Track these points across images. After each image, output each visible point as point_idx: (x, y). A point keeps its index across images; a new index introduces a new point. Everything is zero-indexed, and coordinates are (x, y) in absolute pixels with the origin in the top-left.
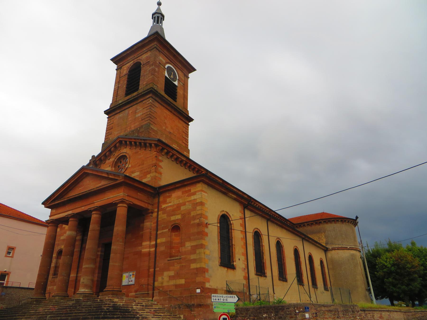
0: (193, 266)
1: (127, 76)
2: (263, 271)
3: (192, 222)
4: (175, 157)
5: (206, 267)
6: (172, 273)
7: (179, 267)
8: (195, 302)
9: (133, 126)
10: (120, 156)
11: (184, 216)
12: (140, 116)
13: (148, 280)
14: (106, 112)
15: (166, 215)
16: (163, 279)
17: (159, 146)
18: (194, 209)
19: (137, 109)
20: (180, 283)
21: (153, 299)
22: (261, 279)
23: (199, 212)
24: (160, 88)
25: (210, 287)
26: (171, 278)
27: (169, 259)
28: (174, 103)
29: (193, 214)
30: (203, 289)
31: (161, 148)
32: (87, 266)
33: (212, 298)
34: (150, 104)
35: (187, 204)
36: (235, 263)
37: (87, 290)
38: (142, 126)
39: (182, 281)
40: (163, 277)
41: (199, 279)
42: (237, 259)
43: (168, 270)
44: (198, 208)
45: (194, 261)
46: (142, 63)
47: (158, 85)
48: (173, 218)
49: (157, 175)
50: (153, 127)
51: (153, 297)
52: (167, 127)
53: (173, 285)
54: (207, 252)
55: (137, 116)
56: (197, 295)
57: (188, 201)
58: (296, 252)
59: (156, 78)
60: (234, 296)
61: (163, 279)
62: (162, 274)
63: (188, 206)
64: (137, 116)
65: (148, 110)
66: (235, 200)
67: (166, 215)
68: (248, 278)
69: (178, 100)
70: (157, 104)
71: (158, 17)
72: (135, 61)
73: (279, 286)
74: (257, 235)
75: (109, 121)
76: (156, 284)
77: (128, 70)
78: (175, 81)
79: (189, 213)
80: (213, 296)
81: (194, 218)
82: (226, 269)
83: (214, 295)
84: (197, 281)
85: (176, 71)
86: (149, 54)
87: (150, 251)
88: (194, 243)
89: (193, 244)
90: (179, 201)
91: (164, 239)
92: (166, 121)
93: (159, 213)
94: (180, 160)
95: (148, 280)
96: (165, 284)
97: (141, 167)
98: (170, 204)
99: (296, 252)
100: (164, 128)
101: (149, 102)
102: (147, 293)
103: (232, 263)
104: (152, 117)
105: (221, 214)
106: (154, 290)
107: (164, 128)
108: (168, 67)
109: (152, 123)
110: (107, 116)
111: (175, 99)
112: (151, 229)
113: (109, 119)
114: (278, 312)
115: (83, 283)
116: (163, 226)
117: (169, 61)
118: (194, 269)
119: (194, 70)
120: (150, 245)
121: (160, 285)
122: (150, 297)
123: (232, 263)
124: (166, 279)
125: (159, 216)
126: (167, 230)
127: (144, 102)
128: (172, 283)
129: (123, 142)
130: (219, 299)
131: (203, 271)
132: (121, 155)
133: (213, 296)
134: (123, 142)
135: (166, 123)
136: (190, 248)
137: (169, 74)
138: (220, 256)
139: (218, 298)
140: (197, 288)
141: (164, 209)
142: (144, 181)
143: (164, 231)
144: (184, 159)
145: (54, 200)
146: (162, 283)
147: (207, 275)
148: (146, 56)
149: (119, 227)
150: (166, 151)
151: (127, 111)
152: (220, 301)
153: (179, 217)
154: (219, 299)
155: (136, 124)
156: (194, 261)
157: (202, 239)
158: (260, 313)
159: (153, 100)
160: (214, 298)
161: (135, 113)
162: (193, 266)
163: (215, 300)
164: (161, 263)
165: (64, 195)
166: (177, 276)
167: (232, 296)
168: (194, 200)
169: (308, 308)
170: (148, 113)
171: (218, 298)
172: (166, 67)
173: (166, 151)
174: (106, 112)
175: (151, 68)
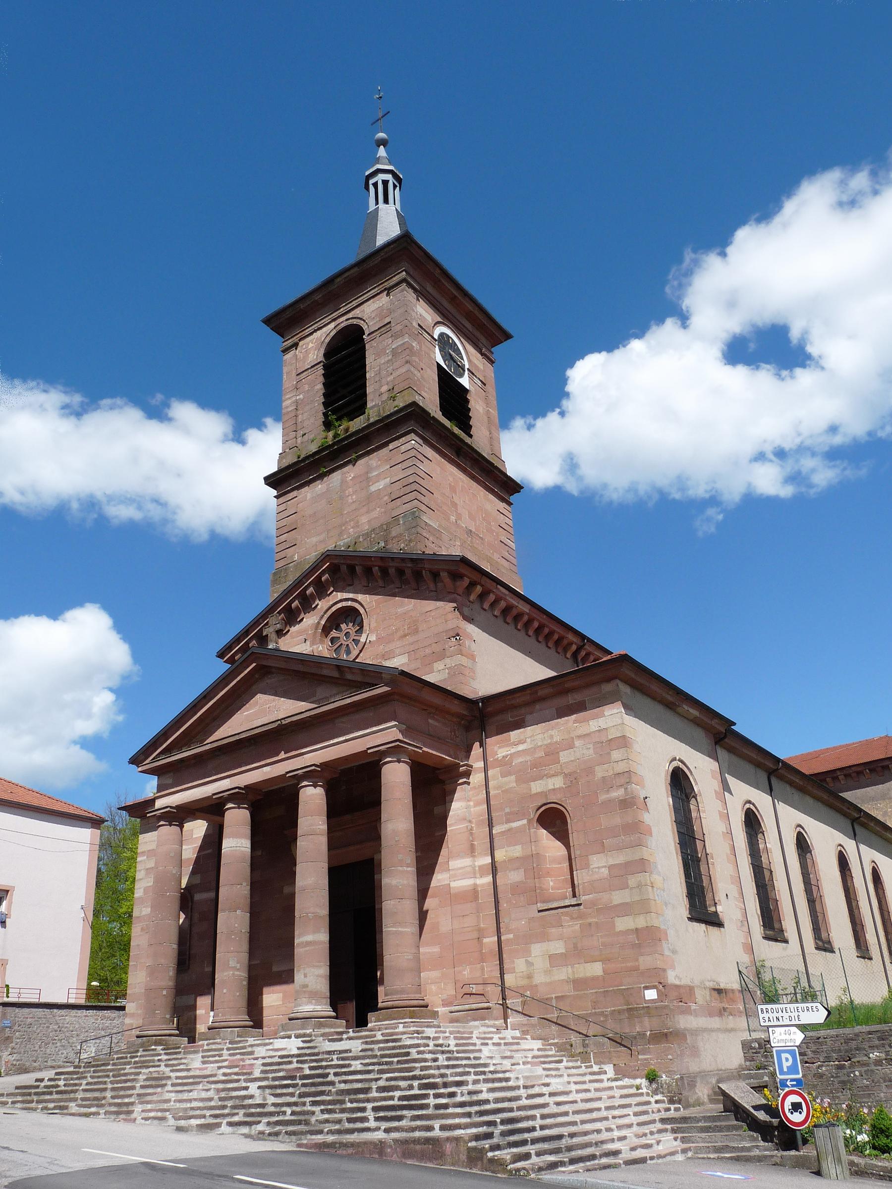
0: (623, 924)
1: (320, 371)
2: (776, 926)
3: (603, 797)
4: (503, 604)
6: (558, 947)
7: (577, 927)
8: (646, 1026)
9: (364, 520)
10: (334, 609)
11: (572, 778)
12: (385, 488)
14: (272, 481)
15: (513, 777)
16: (529, 964)
17: (461, 576)
18: (604, 758)
19: (370, 469)
20: (589, 974)
21: (506, 1022)
22: (776, 948)
23: (621, 767)
24: (430, 399)
25: (677, 982)
26: (554, 960)
27: (541, 906)
28: (468, 440)
29: (600, 772)
30: (664, 988)
31: (467, 581)
33: (761, 1016)
35: (577, 743)
36: (719, 909)
37: (319, 1008)
38: (395, 518)
39: (596, 969)
40: (529, 959)
41: (645, 962)
42: (720, 896)
43: (544, 937)
44: (616, 755)
45: (625, 909)
46: (365, 327)
47: (424, 394)
48: (537, 787)
49: (464, 661)
51: (505, 1018)
52: (459, 516)
53: (567, 981)
54: (656, 878)
55: (373, 488)
56: (649, 1009)
57: (579, 737)
58: (843, 862)
59: (416, 372)
61: (529, 964)
62: (528, 952)
63: (583, 751)
64: (373, 488)
66: (696, 722)
67: (513, 777)
68: (750, 949)
69: (473, 431)
71: (385, 183)
72: (343, 322)
73: (818, 961)
74: (752, 822)
75: (282, 507)
76: (509, 979)
77: (322, 351)
78: (461, 376)
79: (589, 770)
81: (607, 784)
84: (642, 968)
87: (475, 885)
88: (619, 858)
89: (611, 862)
90: (552, 737)
91: (519, 848)
93: (490, 773)
94: (514, 612)
95: (483, 969)
96: (539, 979)
97: (410, 639)
98: (521, 747)
99: (843, 862)
101: (408, 446)
103: (713, 909)
104: (423, 491)
105: (671, 769)
107: (453, 518)
108: (442, 335)
109: (424, 508)
110: (275, 492)
111: (466, 427)
112: (470, 822)
113: (282, 500)
116: (507, 810)
118: (628, 932)
119: (508, 336)
120: (474, 867)
121: (524, 982)
122: (496, 1019)
125: (491, 784)
126: (525, 822)
127: (391, 446)
128: (563, 974)
129: (344, 568)
130: (778, 1019)
131: (649, 937)
132: (339, 605)
134: (344, 568)
135: (455, 505)
136: (605, 871)
137: (448, 357)
139: (775, 1015)
140: (647, 988)
141: (505, 763)
142: (430, 678)
143: (515, 825)
145: (168, 751)
146: (530, 977)
147: (666, 948)
149: (397, 820)
150: (479, 589)
151: (336, 476)
153: (557, 782)
154: (778, 1019)
155: (375, 514)
156: (625, 909)
157: (640, 844)
160: (766, 1015)
161: (366, 479)
162: (623, 924)
164: (517, 919)
166: (576, 953)
173: (479, 589)
174: (272, 481)
175: (399, 342)
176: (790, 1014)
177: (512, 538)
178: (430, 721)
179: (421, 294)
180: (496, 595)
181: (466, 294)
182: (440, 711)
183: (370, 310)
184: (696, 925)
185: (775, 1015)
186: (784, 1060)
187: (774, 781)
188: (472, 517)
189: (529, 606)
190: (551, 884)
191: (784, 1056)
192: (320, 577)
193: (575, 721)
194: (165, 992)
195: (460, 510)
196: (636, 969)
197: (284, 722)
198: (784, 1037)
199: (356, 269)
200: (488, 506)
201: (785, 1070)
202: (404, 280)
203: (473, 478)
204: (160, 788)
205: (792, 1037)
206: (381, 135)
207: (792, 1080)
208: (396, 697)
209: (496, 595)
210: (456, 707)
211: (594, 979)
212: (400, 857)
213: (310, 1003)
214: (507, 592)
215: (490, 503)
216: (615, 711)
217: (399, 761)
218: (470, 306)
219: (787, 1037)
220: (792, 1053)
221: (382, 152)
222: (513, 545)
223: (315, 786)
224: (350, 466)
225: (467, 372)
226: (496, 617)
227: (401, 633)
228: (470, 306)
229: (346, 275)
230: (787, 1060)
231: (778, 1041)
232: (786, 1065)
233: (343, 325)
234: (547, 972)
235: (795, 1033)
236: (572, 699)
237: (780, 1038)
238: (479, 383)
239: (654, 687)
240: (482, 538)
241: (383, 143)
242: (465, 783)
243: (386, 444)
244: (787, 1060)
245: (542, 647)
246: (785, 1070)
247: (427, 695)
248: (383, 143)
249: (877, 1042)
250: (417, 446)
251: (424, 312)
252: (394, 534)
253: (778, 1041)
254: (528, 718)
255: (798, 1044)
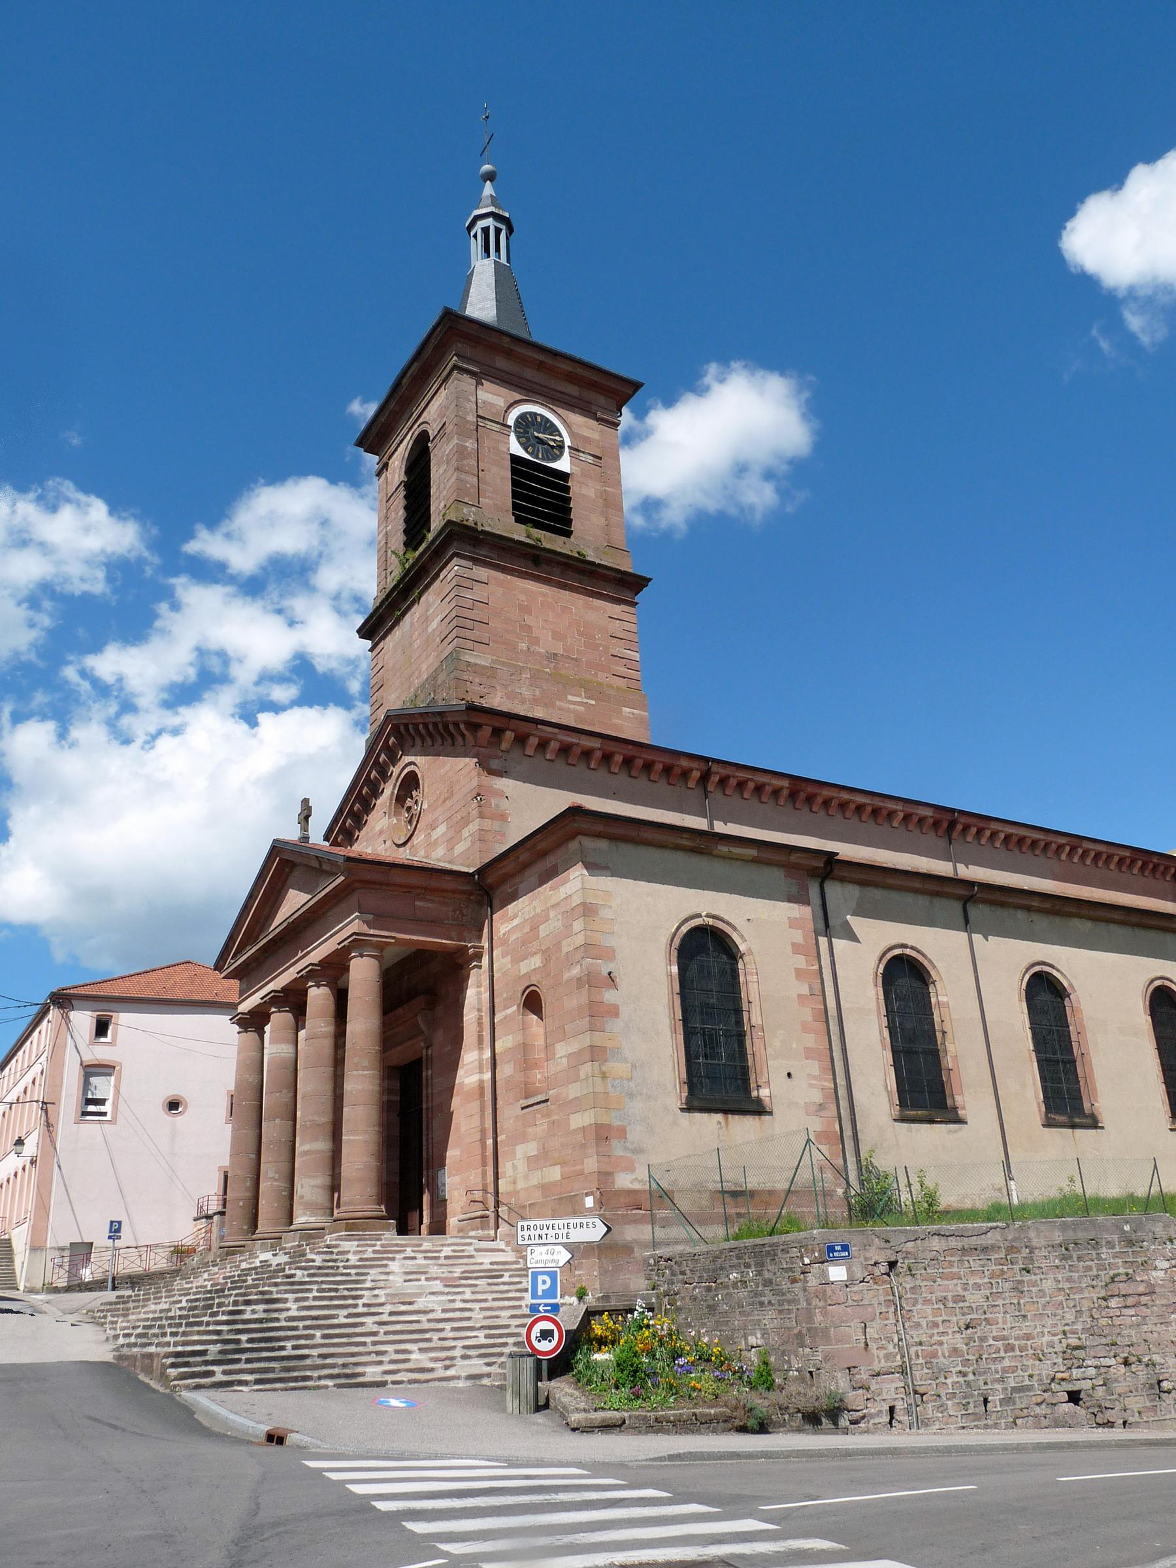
1: (402, 492)
3: (566, 976)
5: (616, 1123)
6: (532, 1148)
7: (545, 1126)
9: (424, 667)
13: (484, 1173)
16: (515, 1167)
24: (496, 512)
32: (307, 1147)
33: (520, 1233)
34: (454, 583)
35: (552, 914)
36: (764, 1093)
37: (313, 1219)
49: (487, 824)
50: (472, 660)
52: (535, 641)
60: (591, 1220)
61: (515, 1167)
62: (514, 1153)
65: (453, 604)
70: (482, 573)
78: (556, 458)
79: (558, 946)
80: (522, 1227)
82: (719, 1117)
83: (525, 1224)
85: (564, 421)
86: (443, 393)
92: (530, 620)
97: (448, 803)
100: (523, 646)
102: (482, 1217)
104: (469, 624)
106: (497, 1204)
108: (523, 416)
109: (469, 644)
114: (762, 1265)
115: (302, 1197)
117: (518, 397)
123: (754, 1094)
124: (522, 1166)
127: (441, 577)
130: (540, 1237)
133: (522, 1227)
136: (564, 1060)
138: (684, 1076)
140: (587, 1194)
144: (595, 743)
148: (436, 407)
152: (544, 1241)
153: (536, 962)
154: (530, 1238)
155: (431, 660)
158: (721, 1268)
159: (464, 562)
160: (526, 1233)
163: (530, 1238)
165: (259, 935)
167: (584, 1221)
168: (566, 898)
169: (845, 1248)
170: (453, 614)
171: (539, 1232)
172: (511, 421)
173: (509, 735)
176: (557, 1231)
177: (634, 646)
178: (417, 903)
179: (478, 378)
180: (540, 738)
181: (555, 354)
182: (426, 892)
183: (437, 409)
184: (698, 1116)
185: (539, 1232)
186: (540, 1282)
187: (973, 911)
188: (557, 636)
189: (600, 740)
190: (539, 1076)
191: (540, 1278)
192: (387, 741)
193: (552, 889)
194: (241, 1204)
195: (536, 633)
196: (581, 1173)
197: (290, 920)
198: (544, 1257)
199: (415, 364)
200: (591, 616)
201: (540, 1293)
202: (455, 367)
203: (564, 587)
204: (241, 993)
205: (555, 1257)
206: (487, 167)
207: (546, 1305)
208: (357, 885)
209: (540, 738)
210: (448, 884)
211: (555, 1184)
212: (356, 1060)
213: (305, 1214)
214: (557, 731)
215: (600, 613)
216: (578, 873)
217: (361, 956)
218: (565, 367)
219: (549, 1257)
220: (553, 1276)
221: (488, 189)
222: (637, 656)
223: (318, 986)
224: (416, 606)
225: (567, 450)
226: (552, 761)
227: (442, 799)
228: (565, 367)
229: (409, 374)
230: (544, 1282)
231: (537, 1262)
232: (541, 1288)
233: (416, 433)
234: (526, 1177)
235: (559, 1253)
236: (549, 861)
237: (539, 1258)
238: (590, 459)
239: (649, 835)
240: (576, 660)
241: (490, 177)
242: (475, 966)
243: (437, 575)
244: (544, 1282)
245: (642, 783)
246: (540, 1293)
247: (397, 877)
248: (490, 177)
249: (735, 1261)
250: (462, 571)
251: (492, 396)
252: (439, 682)
253: (537, 1262)
254: (521, 886)
255: (561, 1264)
